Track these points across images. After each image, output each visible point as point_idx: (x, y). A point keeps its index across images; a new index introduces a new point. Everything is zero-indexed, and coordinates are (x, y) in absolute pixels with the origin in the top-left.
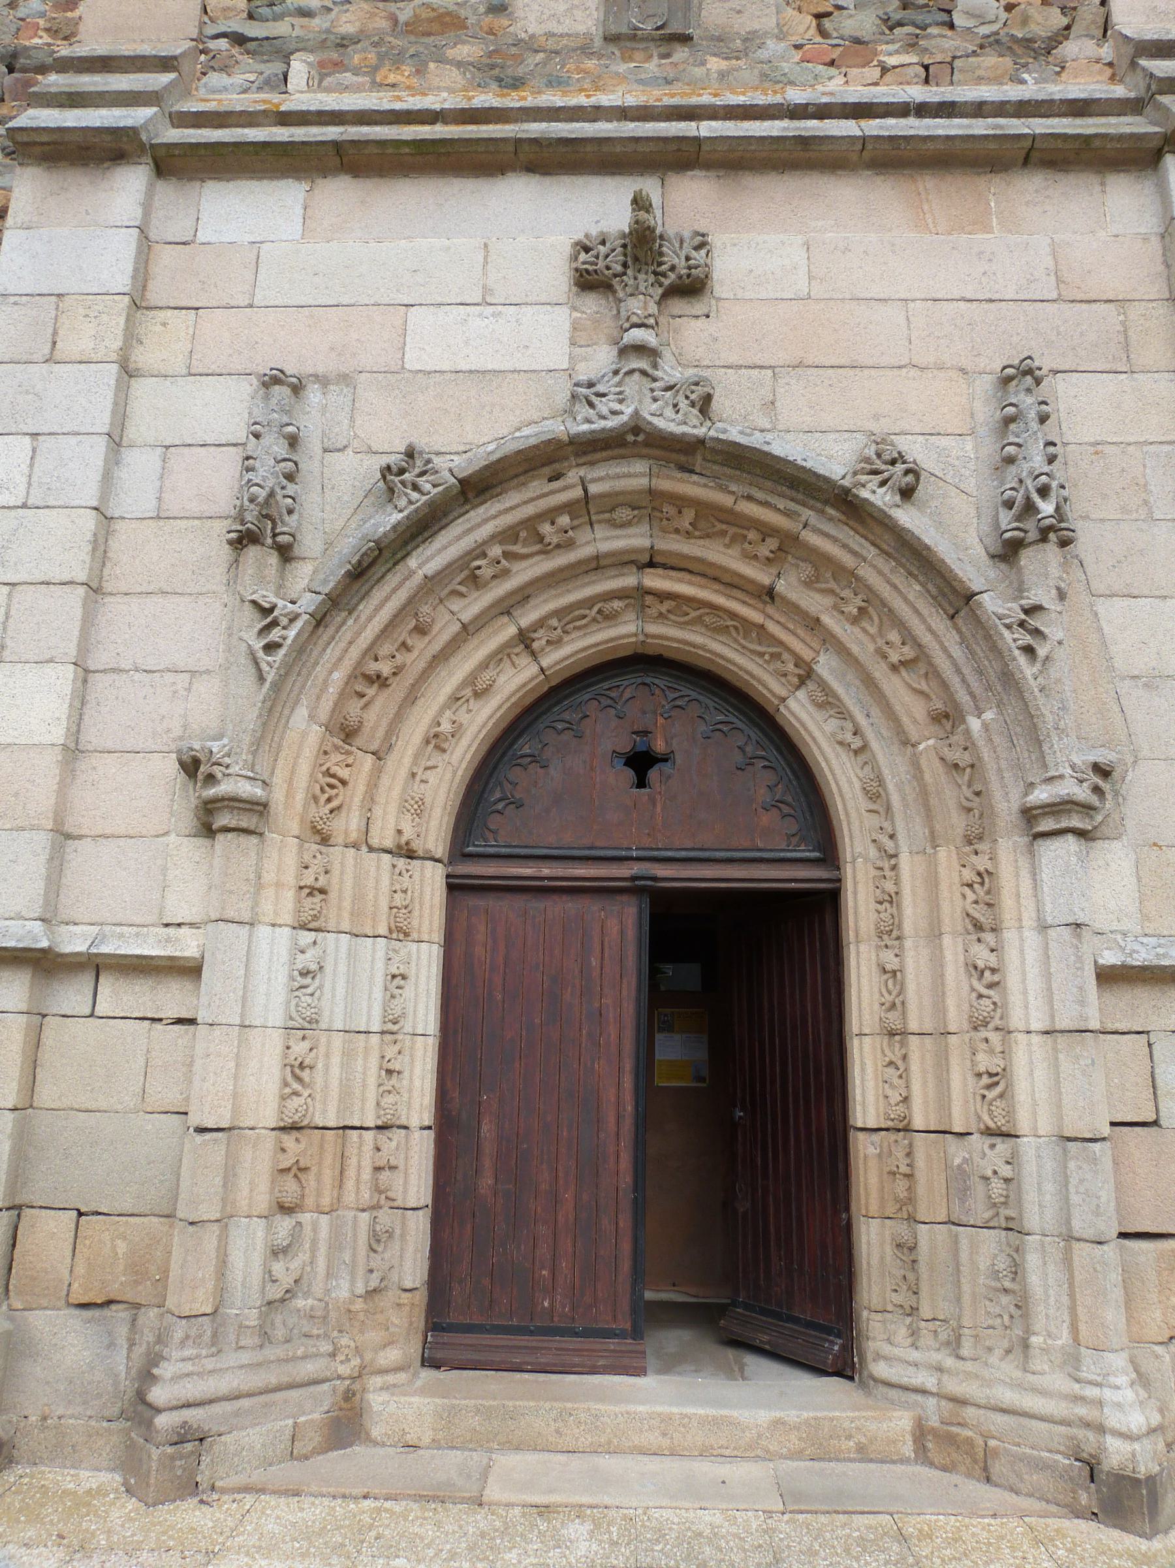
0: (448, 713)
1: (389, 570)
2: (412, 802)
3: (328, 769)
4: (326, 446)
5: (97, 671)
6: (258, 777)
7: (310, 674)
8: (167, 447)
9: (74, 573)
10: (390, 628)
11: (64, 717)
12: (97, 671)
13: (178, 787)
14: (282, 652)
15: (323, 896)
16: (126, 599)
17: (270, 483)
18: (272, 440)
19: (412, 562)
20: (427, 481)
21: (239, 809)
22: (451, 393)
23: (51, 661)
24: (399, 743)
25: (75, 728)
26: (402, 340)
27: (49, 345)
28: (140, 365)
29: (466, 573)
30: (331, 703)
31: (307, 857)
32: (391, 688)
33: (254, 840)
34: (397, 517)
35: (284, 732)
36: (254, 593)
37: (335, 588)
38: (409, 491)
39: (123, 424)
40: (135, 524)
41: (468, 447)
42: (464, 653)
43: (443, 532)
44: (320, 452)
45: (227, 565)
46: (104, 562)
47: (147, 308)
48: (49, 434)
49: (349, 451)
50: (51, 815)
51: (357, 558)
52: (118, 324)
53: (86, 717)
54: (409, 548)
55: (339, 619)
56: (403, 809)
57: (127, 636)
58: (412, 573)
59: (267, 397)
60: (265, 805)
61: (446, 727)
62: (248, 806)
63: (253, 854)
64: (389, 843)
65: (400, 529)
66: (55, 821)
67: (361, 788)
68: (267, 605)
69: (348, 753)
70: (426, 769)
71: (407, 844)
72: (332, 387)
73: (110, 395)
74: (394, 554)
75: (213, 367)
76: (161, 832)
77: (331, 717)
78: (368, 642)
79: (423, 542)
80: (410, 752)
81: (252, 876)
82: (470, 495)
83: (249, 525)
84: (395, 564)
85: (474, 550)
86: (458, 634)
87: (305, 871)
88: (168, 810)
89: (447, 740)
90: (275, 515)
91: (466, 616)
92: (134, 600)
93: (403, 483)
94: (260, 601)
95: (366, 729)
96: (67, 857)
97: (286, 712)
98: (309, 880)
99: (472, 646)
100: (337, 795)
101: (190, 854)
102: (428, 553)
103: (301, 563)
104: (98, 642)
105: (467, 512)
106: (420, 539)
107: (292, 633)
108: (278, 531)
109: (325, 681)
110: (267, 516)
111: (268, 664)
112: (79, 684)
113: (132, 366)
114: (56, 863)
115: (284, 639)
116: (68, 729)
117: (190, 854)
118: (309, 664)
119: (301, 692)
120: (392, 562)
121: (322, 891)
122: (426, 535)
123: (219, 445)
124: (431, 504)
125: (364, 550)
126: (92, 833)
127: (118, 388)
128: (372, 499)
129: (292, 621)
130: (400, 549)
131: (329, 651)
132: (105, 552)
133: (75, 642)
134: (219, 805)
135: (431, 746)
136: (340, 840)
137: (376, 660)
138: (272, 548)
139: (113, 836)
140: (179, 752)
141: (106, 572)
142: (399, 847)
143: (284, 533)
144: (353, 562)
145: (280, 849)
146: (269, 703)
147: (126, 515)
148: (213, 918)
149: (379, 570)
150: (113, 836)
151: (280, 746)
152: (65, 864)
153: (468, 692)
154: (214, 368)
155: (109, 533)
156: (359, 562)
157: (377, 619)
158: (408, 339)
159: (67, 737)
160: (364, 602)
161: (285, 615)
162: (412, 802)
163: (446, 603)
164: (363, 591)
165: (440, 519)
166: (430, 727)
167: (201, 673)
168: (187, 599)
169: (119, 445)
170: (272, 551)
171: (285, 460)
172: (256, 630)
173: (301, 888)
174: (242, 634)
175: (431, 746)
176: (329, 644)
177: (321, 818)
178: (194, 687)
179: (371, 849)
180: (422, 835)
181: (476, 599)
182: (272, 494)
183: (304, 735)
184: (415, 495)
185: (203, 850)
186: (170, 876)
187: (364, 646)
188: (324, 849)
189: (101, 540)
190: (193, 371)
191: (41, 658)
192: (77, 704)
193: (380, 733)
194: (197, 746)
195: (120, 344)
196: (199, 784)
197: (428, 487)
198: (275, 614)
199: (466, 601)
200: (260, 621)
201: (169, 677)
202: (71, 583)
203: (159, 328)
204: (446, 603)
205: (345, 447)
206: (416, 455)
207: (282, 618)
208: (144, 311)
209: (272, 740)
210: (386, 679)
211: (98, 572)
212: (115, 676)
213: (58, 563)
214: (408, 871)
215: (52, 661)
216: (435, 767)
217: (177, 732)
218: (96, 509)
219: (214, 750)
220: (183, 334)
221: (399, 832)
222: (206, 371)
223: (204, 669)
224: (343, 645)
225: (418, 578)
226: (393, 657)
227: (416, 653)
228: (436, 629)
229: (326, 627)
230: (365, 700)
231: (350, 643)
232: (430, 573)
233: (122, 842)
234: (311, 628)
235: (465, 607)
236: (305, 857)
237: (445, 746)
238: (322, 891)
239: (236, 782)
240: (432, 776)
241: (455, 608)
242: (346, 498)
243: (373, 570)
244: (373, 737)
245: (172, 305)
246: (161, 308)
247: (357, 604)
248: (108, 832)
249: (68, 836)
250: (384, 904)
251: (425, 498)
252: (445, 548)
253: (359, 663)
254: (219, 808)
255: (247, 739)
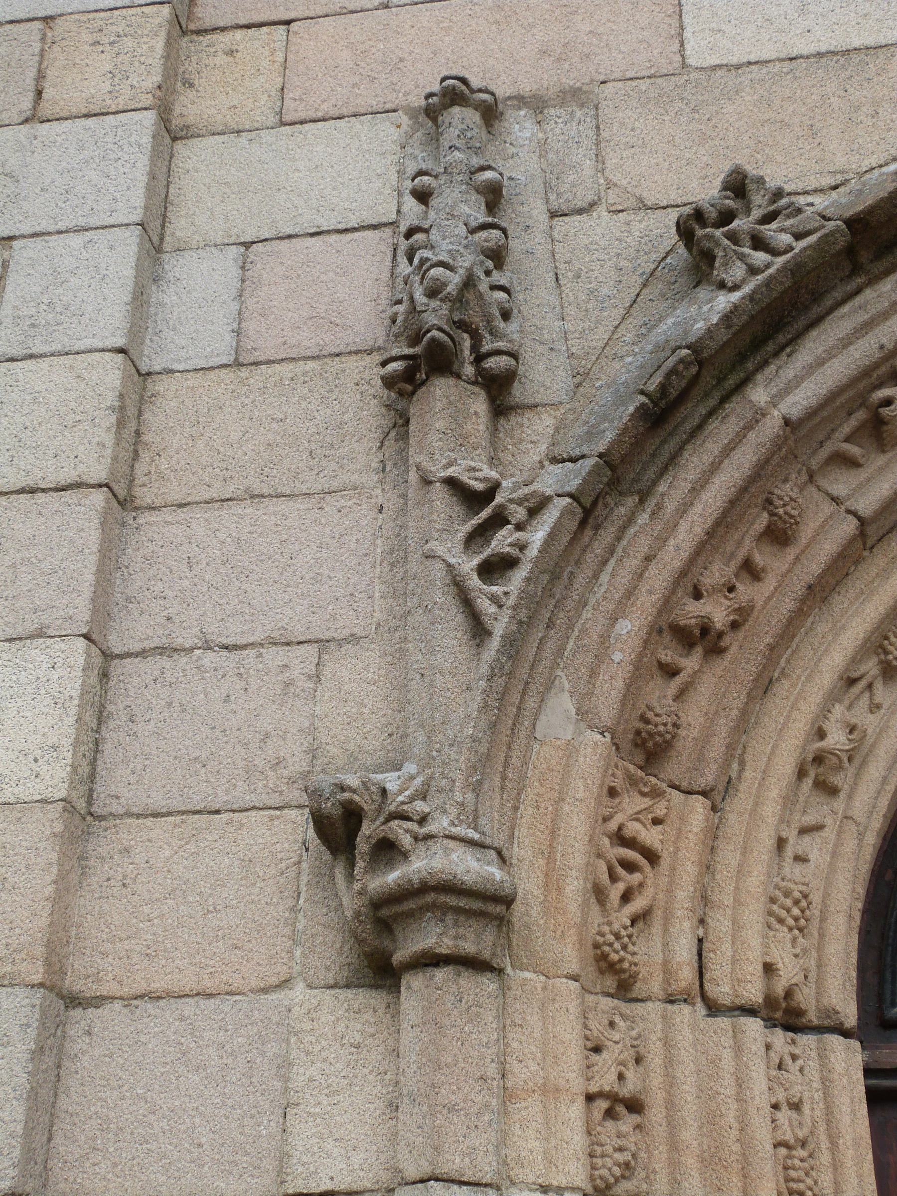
0: (838, 710)
1: (711, 413)
2: (789, 902)
3: (620, 828)
4: (554, 205)
5: (129, 655)
6: (488, 841)
7: (571, 627)
8: (247, 245)
9: (82, 468)
10: (721, 530)
11: (67, 743)
12: (129, 655)
13: (304, 879)
14: (518, 577)
15: (634, 1119)
16: (182, 514)
17: (466, 261)
18: (456, 194)
19: (759, 394)
20: (782, 230)
21: (458, 910)
22: (788, 93)
23: (40, 634)
24: (748, 774)
25: (85, 770)
26: (675, 22)
27: (31, 95)
28: (190, 120)
29: (861, 415)
30: (619, 684)
31: (597, 1026)
32: (728, 656)
33: (488, 984)
34: (724, 301)
35: (529, 748)
36: (450, 464)
37: (616, 442)
38: (747, 250)
39: (164, 216)
40: (193, 380)
41: (839, 178)
42: (859, 585)
43: (814, 333)
44: (545, 217)
45: (378, 435)
46: (136, 452)
47: (199, 32)
48: (35, 235)
49: (602, 210)
50: (39, 950)
51: (658, 379)
52: (152, 49)
53: (107, 748)
54: (750, 366)
55: (622, 510)
56: (772, 920)
57: (186, 583)
58: (760, 414)
59: (434, 139)
60: (508, 901)
61: (836, 738)
62: (476, 905)
63: (489, 1017)
64: (754, 993)
65: (738, 322)
66: (48, 964)
67: (689, 871)
68: (479, 486)
69: (655, 794)
70: (804, 831)
71: (789, 994)
72: (552, 111)
73: (143, 163)
74: (720, 380)
75: (324, 106)
76: (274, 980)
77: (622, 711)
78: (685, 555)
79: (776, 354)
80: (775, 792)
81: (492, 1070)
82: (864, 256)
83: (435, 333)
84: (725, 399)
85: (876, 366)
86: (852, 541)
87: (595, 1057)
88: (287, 931)
89: (840, 768)
90: (477, 321)
91: (867, 504)
92: (198, 513)
93: (733, 237)
94: (465, 478)
95: (688, 737)
96: (73, 1048)
97: (531, 703)
98: (606, 1081)
99: (874, 571)
100: (641, 885)
101: (341, 1027)
102: (789, 372)
103: (528, 414)
104: (129, 600)
105: (858, 291)
106: (770, 347)
107: (537, 536)
108: (486, 348)
109: (605, 638)
110: (462, 325)
111: (494, 599)
112: (94, 679)
113: (176, 122)
114: (49, 1061)
115: (522, 547)
116: (75, 769)
117: (341, 1027)
118: (570, 604)
119: (555, 665)
120: (717, 395)
121: (634, 1106)
122: (781, 338)
123: (346, 231)
124: (795, 270)
125: (670, 363)
126: (125, 991)
127: (156, 154)
128: (657, 287)
129: (533, 512)
130: (733, 368)
131: (604, 578)
132: (138, 433)
133: (87, 593)
134: (411, 904)
135: (809, 782)
136: (656, 986)
137: (697, 595)
138: (475, 383)
139: (170, 995)
140: (315, 794)
141: (141, 469)
142: (770, 1001)
143: (498, 352)
144: (652, 387)
145: (543, 1008)
146: (500, 681)
147: (176, 367)
148: (412, 1172)
149: (694, 411)
150: (170, 995)
151: (523, 778)
152: (66, 1063)
153: (871, 667)
154: (325, 108)
155: (144, 400)
156: (663, 388)
157: (698, 508)
158: (686, 19)
159: (72, 786)
160: (668, 478)
161: (519, 502)
162: (789, 902)
163: (823, 483)
164: (666, 453)
165: (807, 308)
166: (808, 741)
167: (339, 643)
168: (301, 505)
169: (159, 250)
170: (476, 389)
171: (484, 227)
172: (461, 535)
173: (590, 1098)
174: (432, 545)
175: (809, 782)
176: (605, 562)
177: (618, 936)
178: (327, 672)
179: (713, 1009)
180: (812, 976)
181: (881, 470)
182: (469, 283)
183: (570, 750)
184: (760, 257)
185: (368, 1016)
186: (299, 1080)
187: (678, 564)
188: (626, 1008)
189: (131, 411)
190: (287, 118)
191: (20, 631)
192: (90, 719)
193: (716, 750)
194: (353, 781)
195: (157, 79)
196: (360, 864)
197: (786, 239)
198: (499, 499)
199: (862, 474)
200: (465, 522)
201: (274, 656)
202: (78, 485)
203: (221, 59)
204: (823, 483)
205: (592, 205)
206: (751, 187)
207: (512, 507)
208: (195, 37)
209: (506, 764)
210: (720, 635)
211: (126, 469)
212: (165, 662)
213: (51, 453)
214: (794, 1058)
215: (40, 636)
216: (819, 827)
217: (297, 764)
218: (121, 351)
219: (389, 786)
220: (265, 63)
221: (769, 969)
222: (312, 114)
223: (346, 633)
224: (633, 563)
225: (772, 425)
226: (731, 589)
227: (770, 583)
228: (806, 533)
229: (597, 527)
230: (678, 681)
231: (648, 559)
232: (795, 413)
233: (189, 1007)
234: (573, 525)
235: (860, 486)
236: (592, 1024)
237: (837, 780)
238: (634, 1106)
239: (447, 852)
240: (812, 846)
241: (839, 489)
242: (605, 291)
243: (682, 412)
244: (701, 758)
245: (243, 21)
246: (223, 29)
247: (655, 483)
248: (158, 985)
249: (73, 1001)
250: (763, 1137)
251: (780, 261)
252: (821, 362)
253: (667, 604)
254: (410, 914)
255: (462, 759)
